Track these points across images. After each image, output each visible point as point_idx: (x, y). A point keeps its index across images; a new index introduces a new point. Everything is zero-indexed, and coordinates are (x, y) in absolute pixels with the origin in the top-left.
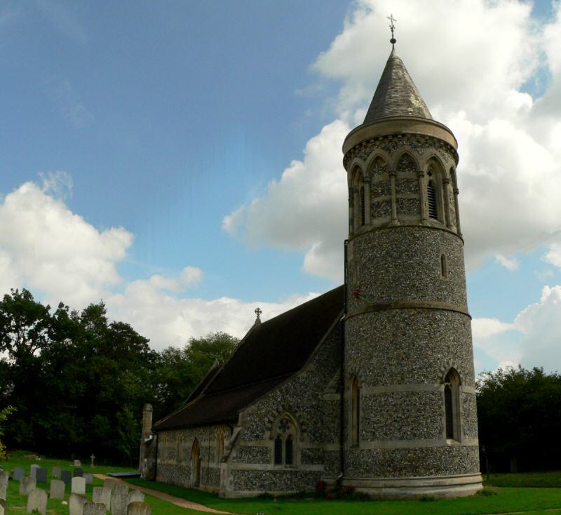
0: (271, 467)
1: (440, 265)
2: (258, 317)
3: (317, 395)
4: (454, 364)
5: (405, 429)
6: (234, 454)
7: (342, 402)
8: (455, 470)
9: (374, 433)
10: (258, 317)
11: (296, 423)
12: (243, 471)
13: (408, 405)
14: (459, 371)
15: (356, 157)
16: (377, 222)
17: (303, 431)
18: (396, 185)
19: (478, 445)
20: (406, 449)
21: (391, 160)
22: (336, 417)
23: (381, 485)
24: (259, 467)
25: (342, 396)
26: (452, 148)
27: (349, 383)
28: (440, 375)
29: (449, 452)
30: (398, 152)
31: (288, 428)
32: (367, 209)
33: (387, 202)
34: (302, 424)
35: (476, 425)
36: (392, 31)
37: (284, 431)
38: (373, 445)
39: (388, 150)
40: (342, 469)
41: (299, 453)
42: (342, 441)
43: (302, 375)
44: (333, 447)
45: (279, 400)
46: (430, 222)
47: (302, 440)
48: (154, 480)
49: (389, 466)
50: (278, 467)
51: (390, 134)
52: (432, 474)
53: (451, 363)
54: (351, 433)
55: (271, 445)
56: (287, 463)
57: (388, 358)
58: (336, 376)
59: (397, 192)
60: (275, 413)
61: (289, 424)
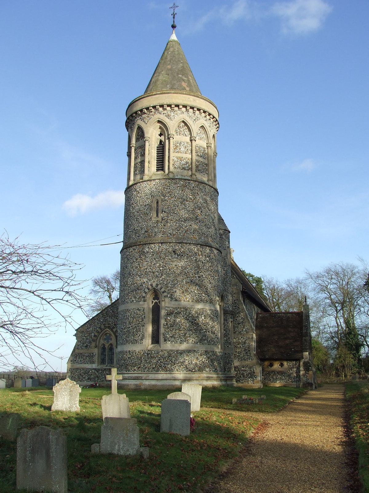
4: (157, 285)
12: (77, 369)
24: (89, 366)
36: (174, 18)
45: (102, 321)
51: (165, 103)
52: (135, 370)
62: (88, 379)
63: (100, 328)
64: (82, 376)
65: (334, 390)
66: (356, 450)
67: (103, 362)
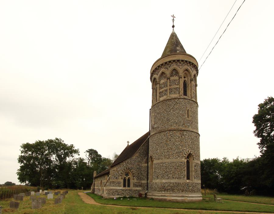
0: (122, 188)
1: (187, 114)
2: (128, 144)
3: (139, 164)
4: (191, 152)
5: (169, 175)
6: (108, 184)
7: (148, 166)
8: (190, 191)
9: (158, 177)
10: (128, 144)
11: (131, 173)
13: (171, 167)
14: (193, 154)
15: (154, 74)
16: (161, 99)
17: (134, 176)
18: (170, 83)
19: (201, 183)
20: (170, 183)
21: (168, 73)
22: (146, 172)
23: (160, 195)
24: (118, 188)
25: (148, 165)
26: (195, 65)
27: (150, 160)
28: (185, 156)
29: (188, 185)
30: (170, 69)
31: (129, 175)
32: (158, 94)
33: (166, 90)
34: (134, 174)
35: (200, 175)
36: (173, 22)
37: (127, 176)
38: (158, 181)
39: (167, 68)
40: (147, 189)
41: (132, 183)
42: (147, 180)
43: (134, 157)
44: (144, 182)
46: (183, 96)
47: (133, 179)
48: (94, 193)
49: (163, 188)
50: (124, 188)
52: (180, 192)
53: (190, 151)
54: (150, 177)
55: (122, 181)
56: (128, 187)
57: (164, 150)
58: (146, 158)
59: (170, 85)
60: (123, 170)
61: (129, 174)
62: (118, 194)
63: (124, 169)
64: (114, 193)
65: (223, 194)
66: (233, 170)
67: (124, 186)
